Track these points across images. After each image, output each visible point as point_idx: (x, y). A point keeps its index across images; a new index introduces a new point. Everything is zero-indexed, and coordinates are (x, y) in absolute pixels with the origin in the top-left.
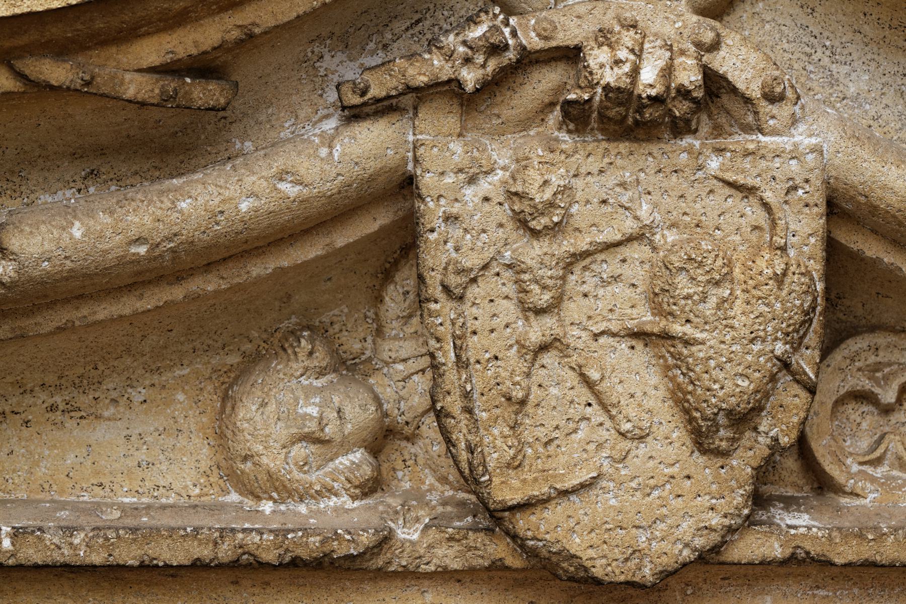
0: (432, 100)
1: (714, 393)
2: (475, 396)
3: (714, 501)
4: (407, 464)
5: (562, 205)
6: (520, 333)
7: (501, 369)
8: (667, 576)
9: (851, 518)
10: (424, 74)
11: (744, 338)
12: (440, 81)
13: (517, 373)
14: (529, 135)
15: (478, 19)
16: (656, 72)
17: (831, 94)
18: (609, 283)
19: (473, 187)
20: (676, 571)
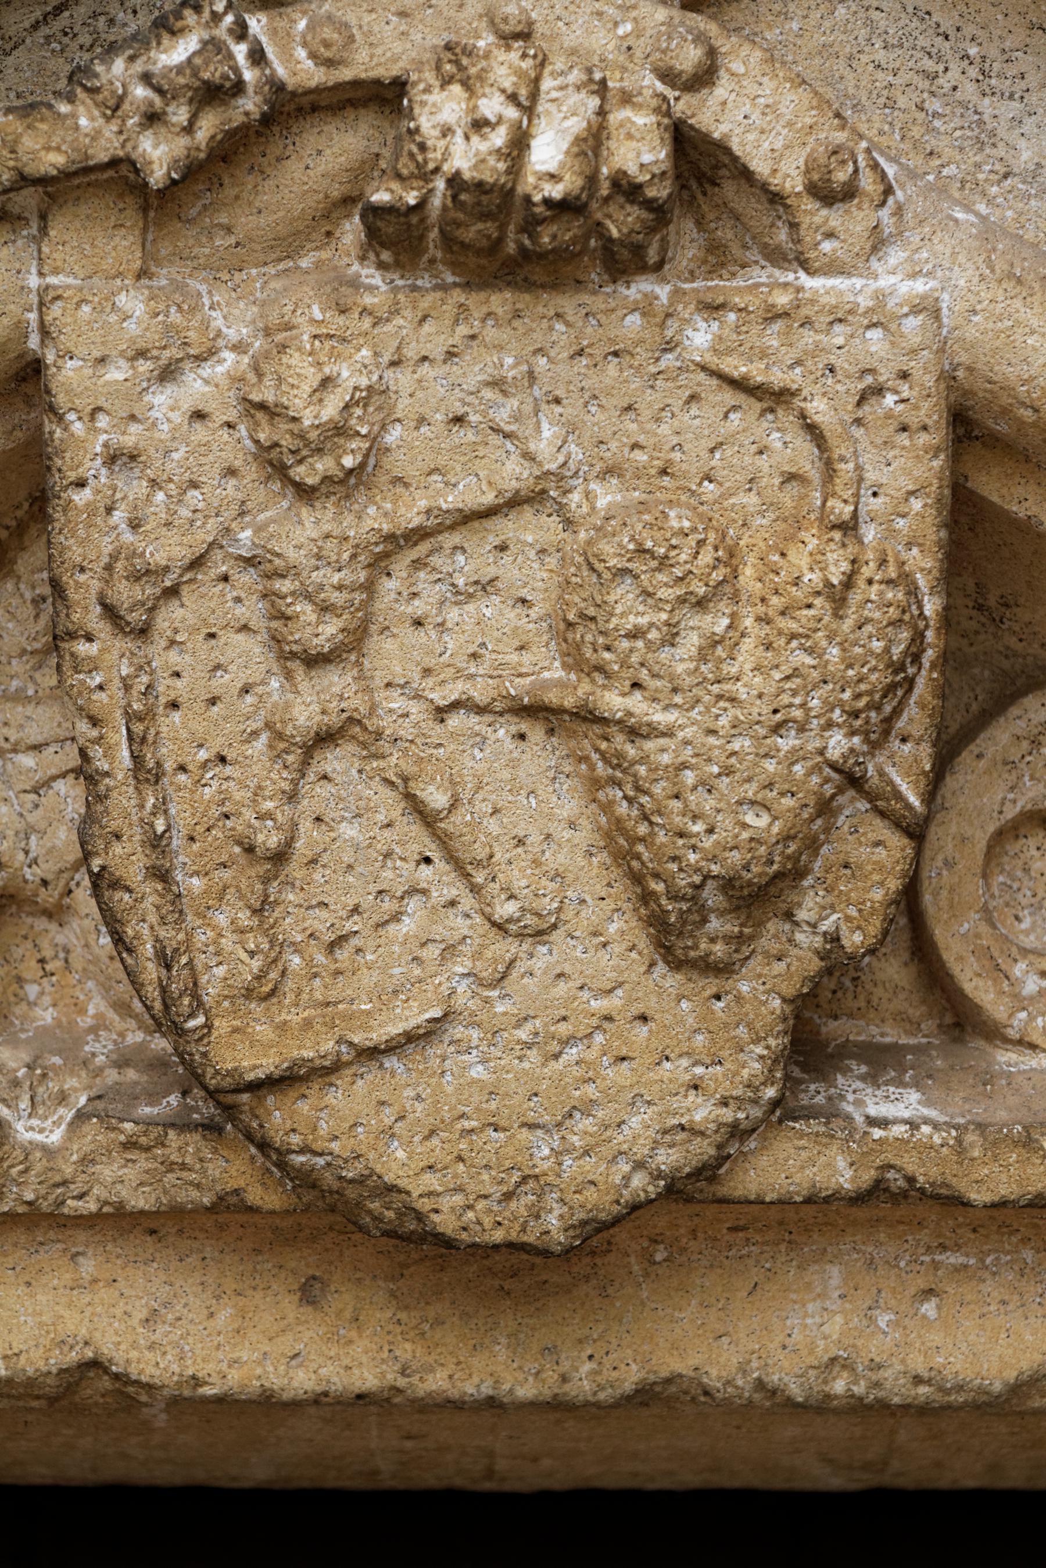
0: (78, 199)
1: (693, 841)
2: (175, 842)
3: (699, 1070)
4: (48, 967)
5: (364, 431)
6: (275, 705)
7: (232, 784)
8: (598, 1231)
9: (1013, 1100)
10: (58, 149)
11: (758, 723)
12: (91, 163)
13: (267, 793)
14: (298, 268)
15: (179, 24)
16: (565, 146)
17: (978, 166)
18: (471, 596)
19: (170, 389)
20: (617, 1221)
